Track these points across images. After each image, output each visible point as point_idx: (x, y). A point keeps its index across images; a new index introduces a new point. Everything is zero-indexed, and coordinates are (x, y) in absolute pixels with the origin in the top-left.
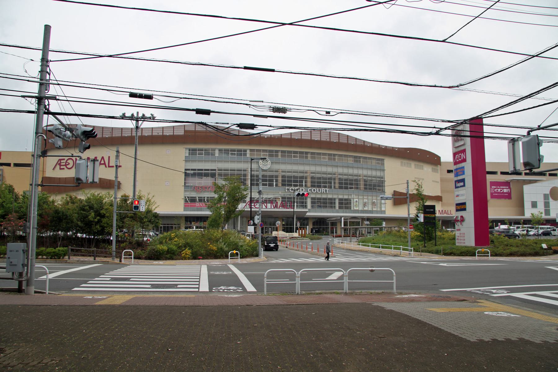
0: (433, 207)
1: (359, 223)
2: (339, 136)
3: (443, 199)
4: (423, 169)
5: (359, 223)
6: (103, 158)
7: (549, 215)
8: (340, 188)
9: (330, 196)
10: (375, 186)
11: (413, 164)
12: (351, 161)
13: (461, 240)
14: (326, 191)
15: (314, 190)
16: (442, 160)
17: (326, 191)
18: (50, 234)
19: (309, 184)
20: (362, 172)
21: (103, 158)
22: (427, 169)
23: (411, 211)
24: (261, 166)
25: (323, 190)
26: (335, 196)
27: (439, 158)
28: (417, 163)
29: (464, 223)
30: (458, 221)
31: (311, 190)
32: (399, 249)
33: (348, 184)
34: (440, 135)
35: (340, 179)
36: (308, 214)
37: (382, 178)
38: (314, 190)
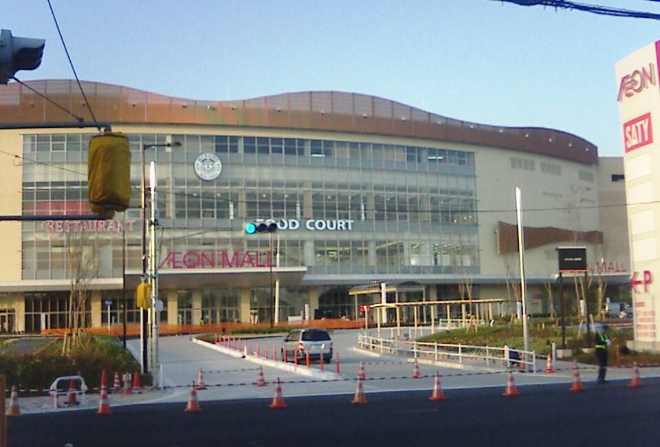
0: (582, 253)
1: (421, 294)
2: (373, 103)
3: (605, 236)
4: (559, 174)
5: (421, 294)
6: (643, 69)
7: (479, 272)
8: (379, 217)
9: (357, 236)
10: (452, 213)
11: (538, 161)
12: (400, 157)
13: (646, 327)
14: (347, 224)
15: (321, 224)
16: (601, 154)
17: (347, 224)
18: (379, 334)
19: (309, 211)
20: (424, 181)
21: (643, 69)
22: (570, 171)
23: (540, 266)
24: (199, 172)
25: (341, 223)
26: (369, 236)
27: (594, 149)
28: (547, 161)
29: (650, 287)
30: (639, 282)
31: (312, 225)
32: (456, 350)
33: (392, 209)
34: (620, 91)
35: (377, 198)
36: (307, 277)
37: (471, 194)
38: (321, 224)
